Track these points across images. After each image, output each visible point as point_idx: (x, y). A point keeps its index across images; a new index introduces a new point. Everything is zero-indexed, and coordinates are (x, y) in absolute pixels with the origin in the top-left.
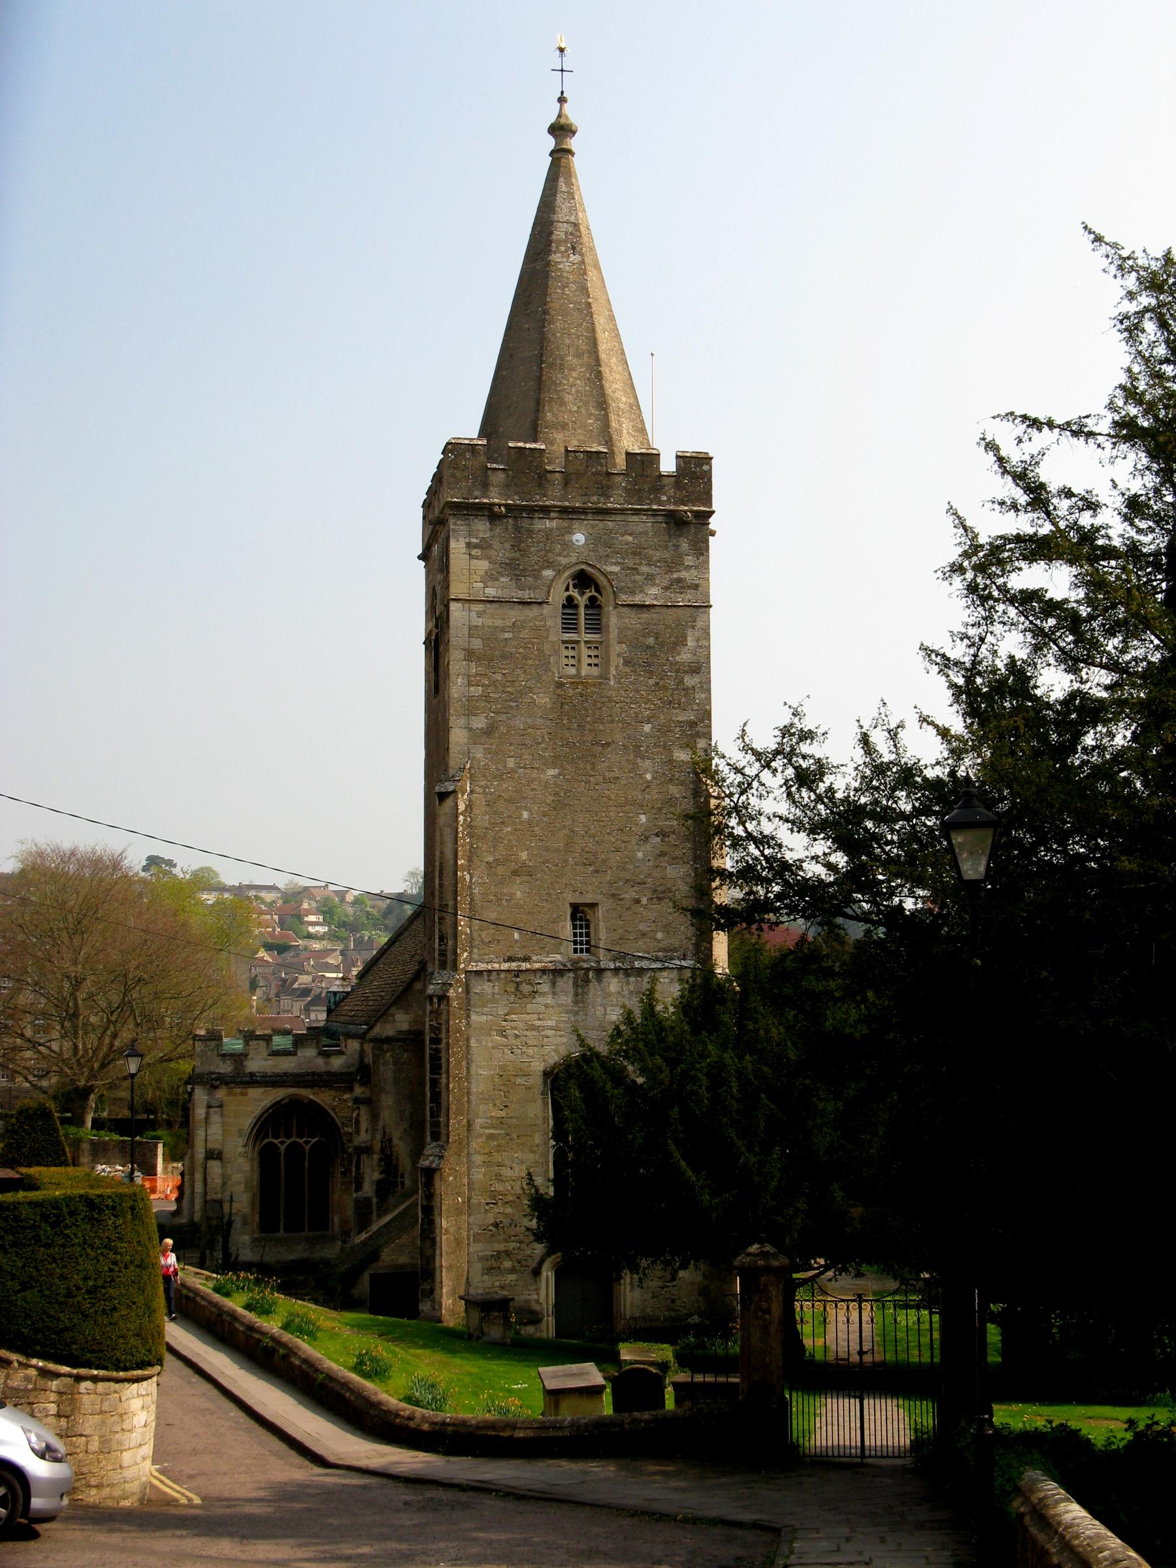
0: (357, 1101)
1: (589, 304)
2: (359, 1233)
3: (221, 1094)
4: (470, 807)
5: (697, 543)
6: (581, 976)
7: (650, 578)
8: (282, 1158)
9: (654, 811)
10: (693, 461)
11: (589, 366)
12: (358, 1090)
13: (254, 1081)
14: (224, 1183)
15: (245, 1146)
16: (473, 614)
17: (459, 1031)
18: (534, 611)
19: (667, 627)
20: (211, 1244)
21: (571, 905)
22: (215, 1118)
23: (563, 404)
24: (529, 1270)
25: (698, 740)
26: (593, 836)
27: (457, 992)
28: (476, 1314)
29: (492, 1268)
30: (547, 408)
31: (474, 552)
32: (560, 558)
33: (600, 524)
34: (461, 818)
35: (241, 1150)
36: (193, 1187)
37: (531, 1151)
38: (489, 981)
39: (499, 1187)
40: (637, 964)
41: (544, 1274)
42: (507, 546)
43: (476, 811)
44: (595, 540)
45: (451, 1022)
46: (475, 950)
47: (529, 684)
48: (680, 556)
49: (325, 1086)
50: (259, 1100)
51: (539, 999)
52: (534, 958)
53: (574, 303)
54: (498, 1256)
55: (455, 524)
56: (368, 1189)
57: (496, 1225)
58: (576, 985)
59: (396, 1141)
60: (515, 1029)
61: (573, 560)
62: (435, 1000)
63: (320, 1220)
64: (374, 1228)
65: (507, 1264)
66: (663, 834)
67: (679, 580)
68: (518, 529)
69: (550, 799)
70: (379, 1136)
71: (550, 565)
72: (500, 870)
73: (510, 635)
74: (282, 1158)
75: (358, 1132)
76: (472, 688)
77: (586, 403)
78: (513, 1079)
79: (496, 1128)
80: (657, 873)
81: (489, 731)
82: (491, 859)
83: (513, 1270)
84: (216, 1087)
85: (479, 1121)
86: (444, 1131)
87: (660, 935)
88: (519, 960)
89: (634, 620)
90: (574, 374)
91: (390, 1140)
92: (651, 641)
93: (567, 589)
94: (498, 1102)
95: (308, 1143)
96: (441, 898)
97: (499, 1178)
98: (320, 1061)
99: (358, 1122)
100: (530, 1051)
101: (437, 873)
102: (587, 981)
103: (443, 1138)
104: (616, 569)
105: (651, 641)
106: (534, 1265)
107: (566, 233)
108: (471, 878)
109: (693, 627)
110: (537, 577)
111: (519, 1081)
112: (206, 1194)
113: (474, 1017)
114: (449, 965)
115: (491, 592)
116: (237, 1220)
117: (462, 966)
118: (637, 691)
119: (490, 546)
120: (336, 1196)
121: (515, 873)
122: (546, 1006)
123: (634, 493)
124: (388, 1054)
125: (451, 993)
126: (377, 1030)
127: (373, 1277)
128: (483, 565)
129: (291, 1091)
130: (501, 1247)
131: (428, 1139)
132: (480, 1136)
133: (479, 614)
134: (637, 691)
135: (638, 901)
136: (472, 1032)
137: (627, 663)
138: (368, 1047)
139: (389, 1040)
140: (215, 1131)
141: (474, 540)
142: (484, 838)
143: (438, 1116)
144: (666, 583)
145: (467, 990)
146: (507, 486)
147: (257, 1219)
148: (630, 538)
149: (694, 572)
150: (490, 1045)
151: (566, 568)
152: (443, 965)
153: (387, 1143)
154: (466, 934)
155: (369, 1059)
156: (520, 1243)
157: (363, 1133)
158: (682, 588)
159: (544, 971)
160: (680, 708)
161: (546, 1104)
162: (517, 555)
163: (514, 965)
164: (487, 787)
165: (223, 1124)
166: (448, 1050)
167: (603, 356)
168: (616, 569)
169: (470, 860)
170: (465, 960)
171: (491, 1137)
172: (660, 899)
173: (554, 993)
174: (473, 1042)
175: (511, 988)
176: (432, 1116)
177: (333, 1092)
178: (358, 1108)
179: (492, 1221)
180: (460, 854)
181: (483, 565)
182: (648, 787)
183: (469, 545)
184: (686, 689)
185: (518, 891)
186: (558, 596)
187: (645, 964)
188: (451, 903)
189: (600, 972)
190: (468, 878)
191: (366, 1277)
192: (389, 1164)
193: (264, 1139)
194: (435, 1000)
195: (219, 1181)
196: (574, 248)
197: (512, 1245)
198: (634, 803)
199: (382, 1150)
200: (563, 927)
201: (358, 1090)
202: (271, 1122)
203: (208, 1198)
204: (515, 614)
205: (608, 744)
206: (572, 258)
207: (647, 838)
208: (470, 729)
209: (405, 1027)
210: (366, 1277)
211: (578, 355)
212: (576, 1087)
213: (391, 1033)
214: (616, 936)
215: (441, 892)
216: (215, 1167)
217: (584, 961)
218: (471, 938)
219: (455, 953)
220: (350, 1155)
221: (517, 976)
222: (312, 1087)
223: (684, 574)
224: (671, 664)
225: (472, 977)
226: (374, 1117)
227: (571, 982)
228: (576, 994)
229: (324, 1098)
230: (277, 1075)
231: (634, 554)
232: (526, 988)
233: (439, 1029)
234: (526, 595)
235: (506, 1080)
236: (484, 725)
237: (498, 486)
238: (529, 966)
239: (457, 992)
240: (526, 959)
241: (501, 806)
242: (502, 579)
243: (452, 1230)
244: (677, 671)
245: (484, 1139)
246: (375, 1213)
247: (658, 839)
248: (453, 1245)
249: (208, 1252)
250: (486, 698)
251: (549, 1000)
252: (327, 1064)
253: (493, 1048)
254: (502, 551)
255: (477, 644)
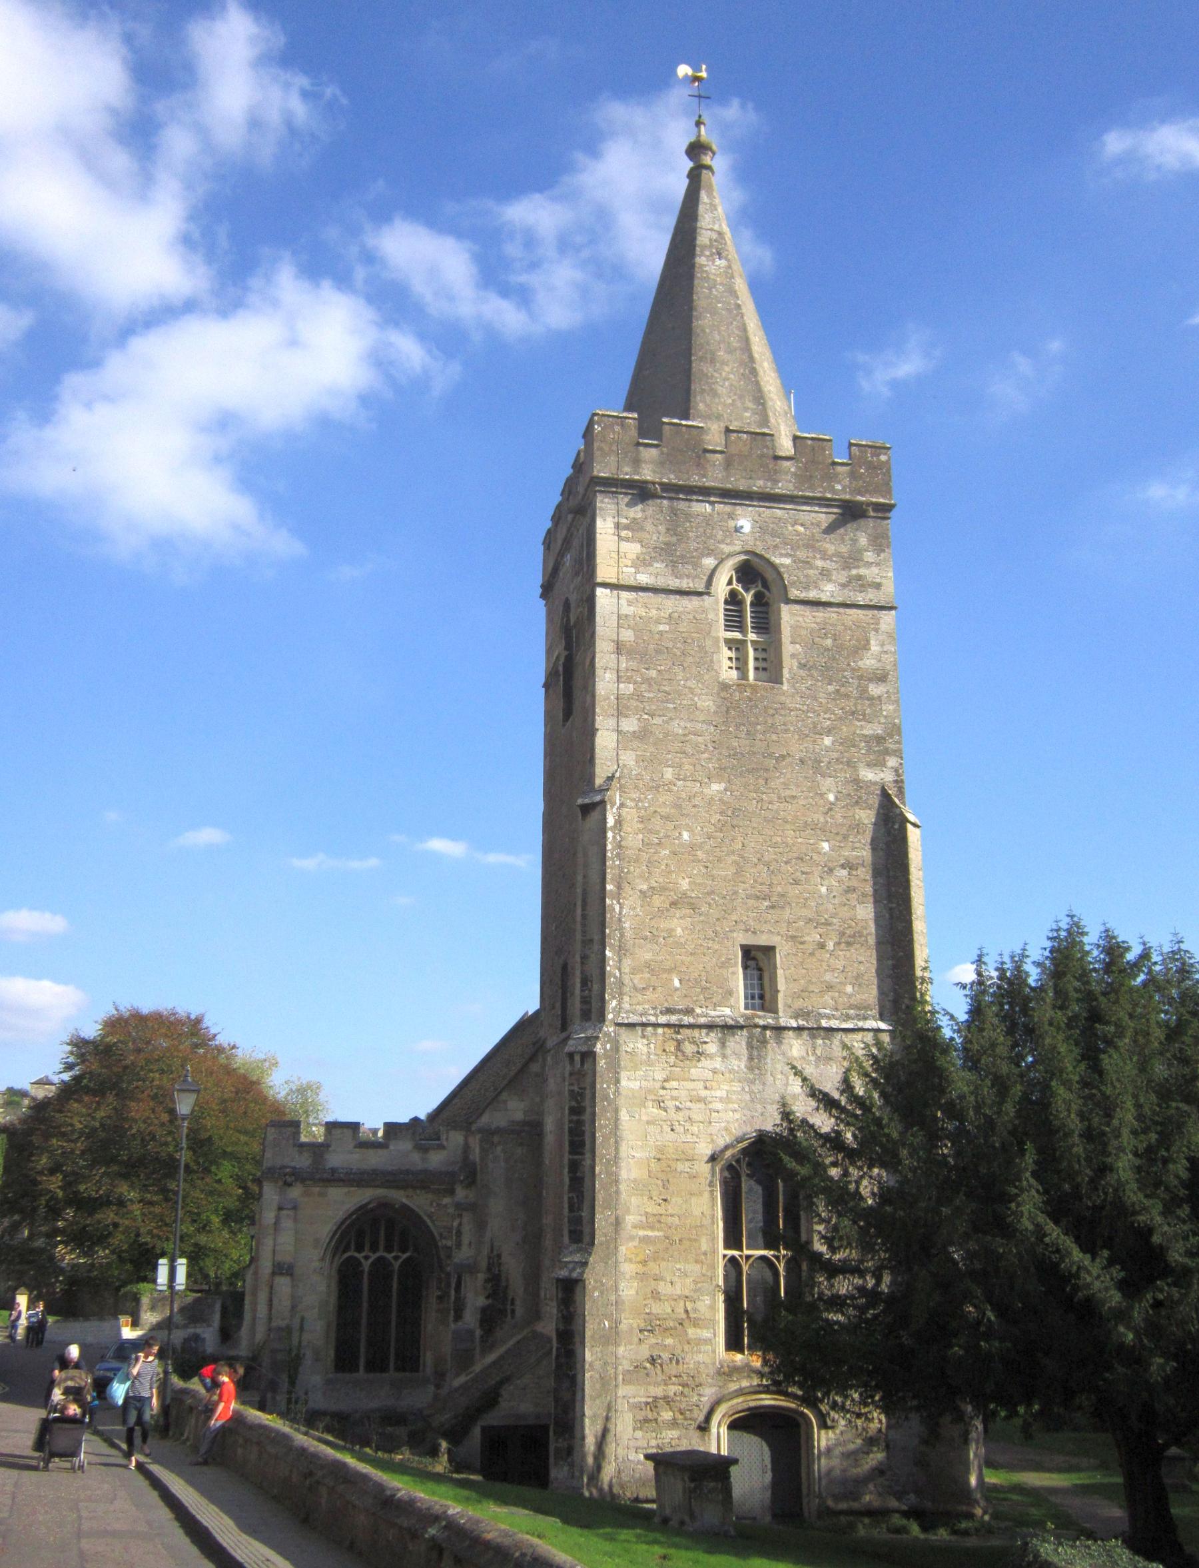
0: (458, 1206)
1: (739, 306)
2: (458, 1375)
3: (296, 1192)
4: (619, 822)
5: (876, 538)
6: (758, 1030)
7: (825, 574)
8: (366, 1276)
9: (839, 838)
10: (869, 450)
11: (742, 363)
12: (461, 1193)
13: (335, 1178)
14: (293, 1307)
15: (322, 1259)
16: (623, 602)
17: (606, 1098)
18: (696, 601)
19: (846, 628)
20: (273, 1386)
21: (742, 947)
22: (287, 1224)
23: (715, 394)
24: (694, 1425)
25: (887, 758)
26: (768, 864)
27: (605, 1049)
28: (678, 1486)
29: (646, 1420)
30: (698, 398)
31: (624, 533)
32: (722, 546)
33: (768, 511)
34: (610, 834)
35: (317, 1264)
36: (254, 1310)
37: (696, 1262)
38: (643, 1037)
39: (656, 1308)
40: (824, 1023)
41: (714, 1430)
42: (662, 528)
43: (626, 828)
44: (762, 529)
45: (598, 1086)
46: (626, 998)
47: (689, 684)
48: (860, 552)
49: (423, 1188)
50: (342, 1202)
51: (705, 1063)
52: (698, 1011)
53: (723, 302)
54: (653, 1404)
55: (602, 502)
56: (471, 1319)
57: (653, 1360)
58: (750, 1046)
59: (506, 1258)
60: (676, 1099)
61: (738, 548)
62: (577, 1058)
63: (409, 1361)
64: (477, 1368)
65: (667, 1415)
66: (849, 866)
67: (859, 578)
68: (674, 512)
69: (716, 818)
70: (485, 1252)
71: (710, 552)
72: (657, 901)
73: (667, 628)
74: (366, 1276)
75: (459, 1245)
76: (622, 686)
77: (741, 397)
78: (673, 1165)
79: (652, 1228)
80: (845, 913)
81: (642, 735)
82: (644, 887)
83: (674, 1424)
84: (290, 1185)
85: (631, 1219)
86: (586, 1230)
87: (849, 989)
88: (679, 1012)
89: (810, 618)
90: (727, 369)
91: (499, 1256)
92: (829, 642)
93: (730, 583)
94: (655, 1194)
95: (396, 1259)
96: (584, 933)
97: (656, 1296)
98: (416, 1157)
99: (459, 1233)
100: (695, 1129)
101: (579, 903)
102: (764, 1042)
103: (586, 1239)
104: (787, 561)
105: (829, 642)
106: (701, 1418)
107: (711, 240)
108: (621, 908)
109: (877, 630)
110: (696, 565)
111: (680, 1166)
112: (270, 1319)
113: (624, 1083)
114: (593, 1016)
115: (644, 579)
116: (309, 1354)
117: (610, 1016)
118: (816, 699)
119: (642, 529)
120: (430, 1327)
121: (673, 904)
122: (715, 1071)
123: (804, 477)
124: (499, 1148)
125: (599, 1048)
126: (485, 1119)
127: (484, 1429)
128: (633, 549)
129: (380, 1192)
130: (659, 1391)
131: (566, 1239)
132: (632, 1238)
133: (630, 603)
134: (816, 699)
135: (822, 946)
136: (621, 1102)
137: (802, 666)
138: (475, 1143)
139: (498, 1131)
140: (286, 1240)
141: (624, 521)
142: (637, 861)
143: (580, 1209)
144: (843, 580)
145: (616, 1048)
146: (662, 464)
147: (332, 1353)
148: (801, 529)
149: (875, 570)
150: (644, 1118)
151: (730, 555)
152: (586, 1015)
153: (495, 1261)
154: (615, 977)
155: (476, 1154)
156: (683, 1386)
157: (465, 1248)
158: (862, 586)
159: (710, 1027)
160: (864, 719)
161: (713, 1199)
162: (674, 539)
163: (674, 1019)
164: (640, 800)
165: (296, 1232)
166: (594, 1121)
167: (756, 356)
168: (787, 561)
169: (619, 887)
170: (614, 1009)
171: (645, 1240)
172: (848, 944)
173: (724, 1056)
174: (624, 1115)
175: (671, 1047)
176: (571, 1209)
177: (430, 1196)
178: (460, 1216)
179: (647, 1355)
180: (609, 877)
181: (633, 549)
182: (831, 809)
183: (617, 526)
184: (871, 699)
185: (678, 925)
186: (721, 588)
187: (834, 1024)
188: (596, 937)
189: (779, 1030)
190: (617, 908)
191: (477, 1431)
192: (496, 1285)
193: (344, 1252)
194: (577, 1058)
195: (287, 1303)
196: (719, 254)
197: (673, 1389)
198: (814, 827)
199: (489, 1269)
200: (734, 973)
201: (461, 1193)
202: (359, 1231)
203: (274, 1324)
204: (671, 604)
205: (783, 757)
206: (718, 262)
207: (831, 870)
208: (619, 732)
209: (519, 1116)
210: (477, 1431)
211: (730, 351)
212: (766, 1175)
213: (503, 1124)
214: (796, 988)
215: (584, 925)
216: (283, 1283)
217: (759, 1017)
218: (620, 983)
219: (603, 1000)
220: (448, 1274)
221: (678, 1033)
222: (404, 1188)
223: (863, 571)
224: (853, 670)
225: (622, 1030)
226: (481, 1226)
227: (744, 1043)
228: (751, 1058)
229: (420, 1202)
230: (363, 1172)
231: (807, 546)
232: (689, 1048)
233: (582, 1095)
234: (685, 584)
235: (665, 1168)
236: (636, 728)
237: (652, 463)
238: (692, 1020)
239: (605, 1049)
240: (689, 1011)
241: (657, 822)
242: (656, 565)
243: (597, 1364)
244: (860, 678)
245: (636, 1243)
246: (478, 1351)
247: (844, 872)
248: (598, 1386)
249: (269, 1395)
250: (639, 697)
251: (717, 1063)
252: (424, 1160)
253: (648, 1123)
254: (656, 534)
255: (627, 635)
